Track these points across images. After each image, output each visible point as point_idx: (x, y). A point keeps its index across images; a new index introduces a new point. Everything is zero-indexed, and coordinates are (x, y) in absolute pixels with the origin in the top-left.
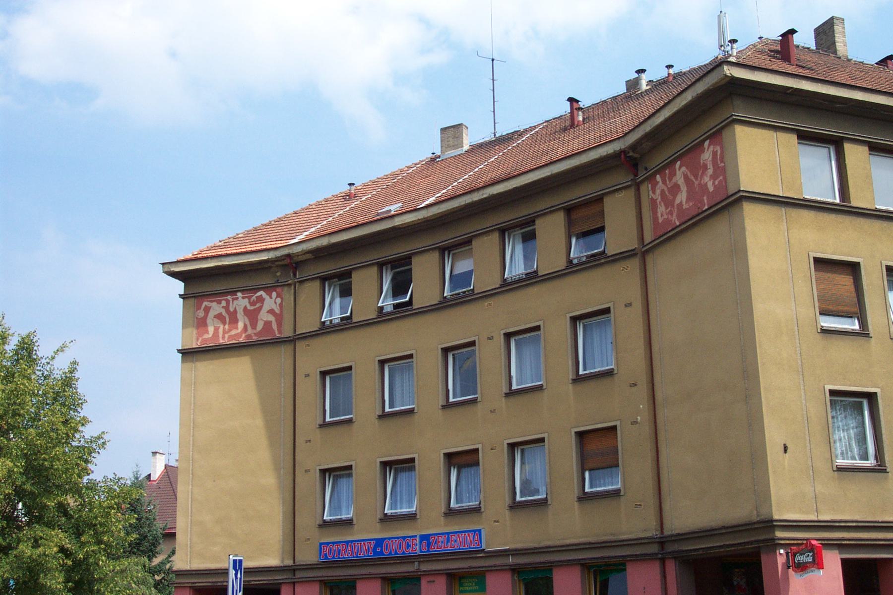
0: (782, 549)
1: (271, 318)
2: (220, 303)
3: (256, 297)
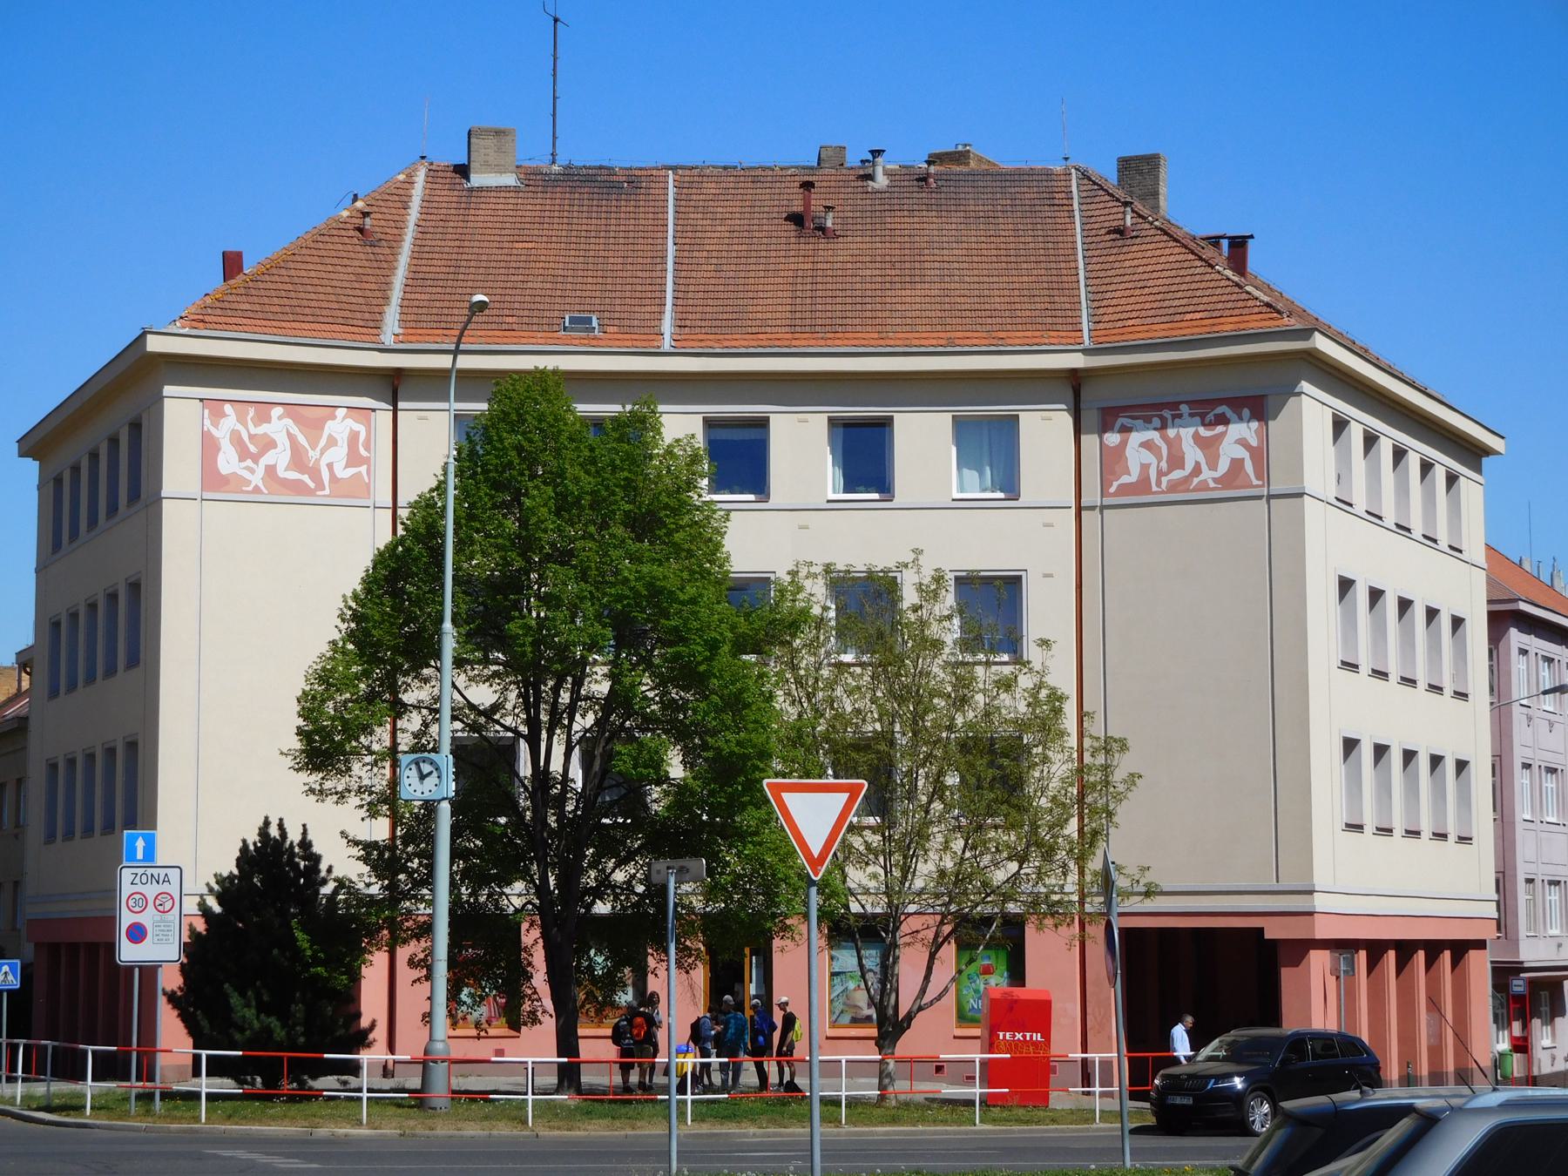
0: (219, 914)
1: (1242, 453)
2: (1151, 422)
3: (1215, 415)
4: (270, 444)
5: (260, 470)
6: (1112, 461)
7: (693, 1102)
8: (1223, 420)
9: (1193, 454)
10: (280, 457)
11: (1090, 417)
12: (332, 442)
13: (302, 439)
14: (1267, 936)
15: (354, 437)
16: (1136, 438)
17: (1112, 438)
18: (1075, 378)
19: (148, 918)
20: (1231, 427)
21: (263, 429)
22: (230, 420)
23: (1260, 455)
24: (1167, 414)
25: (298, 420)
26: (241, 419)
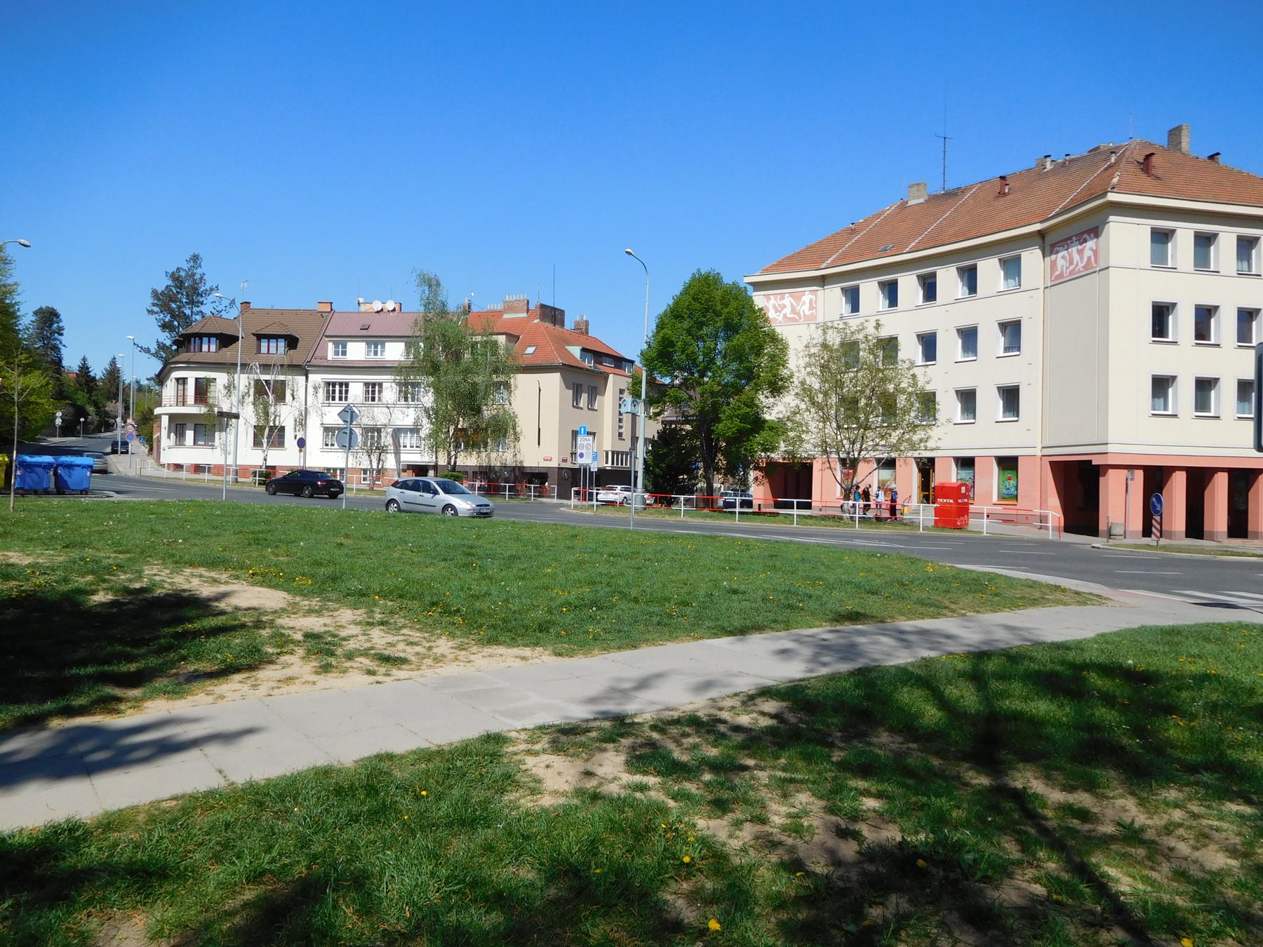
4: (784, 306)
5: (782, 316)
6: (1053, 264)
7: (859, 518)
8: (1085, 241)
9: (1076, 257)
10: (787, 311)
11: (1048, 249)
12: (804, 303)
13: (794, 304)
14: (1093, 463)
15: (811, 301)
16: (1060, 255)
17: (1053, 257)
18: (1041, 234)
19: (584, 451)
20: (1088, 243)
21: (782, 302)
22: (772, 301)
23: (1095, 252)
24: (1069, 242)
25: (794, 298)
26: (776, 300)
